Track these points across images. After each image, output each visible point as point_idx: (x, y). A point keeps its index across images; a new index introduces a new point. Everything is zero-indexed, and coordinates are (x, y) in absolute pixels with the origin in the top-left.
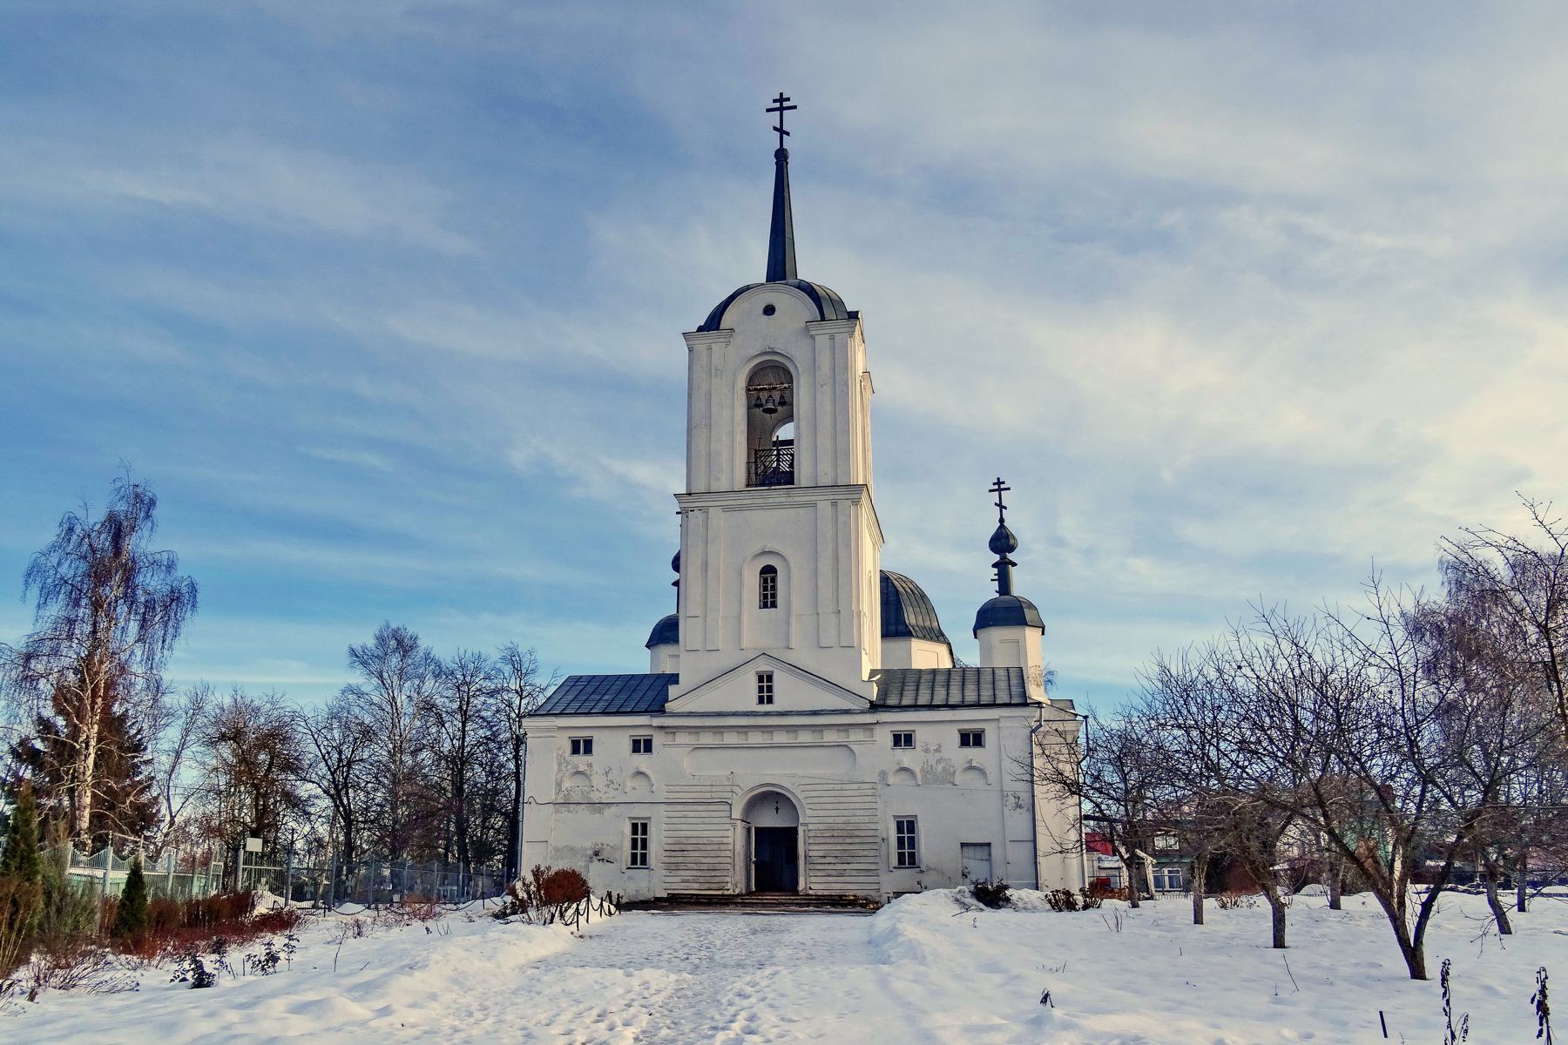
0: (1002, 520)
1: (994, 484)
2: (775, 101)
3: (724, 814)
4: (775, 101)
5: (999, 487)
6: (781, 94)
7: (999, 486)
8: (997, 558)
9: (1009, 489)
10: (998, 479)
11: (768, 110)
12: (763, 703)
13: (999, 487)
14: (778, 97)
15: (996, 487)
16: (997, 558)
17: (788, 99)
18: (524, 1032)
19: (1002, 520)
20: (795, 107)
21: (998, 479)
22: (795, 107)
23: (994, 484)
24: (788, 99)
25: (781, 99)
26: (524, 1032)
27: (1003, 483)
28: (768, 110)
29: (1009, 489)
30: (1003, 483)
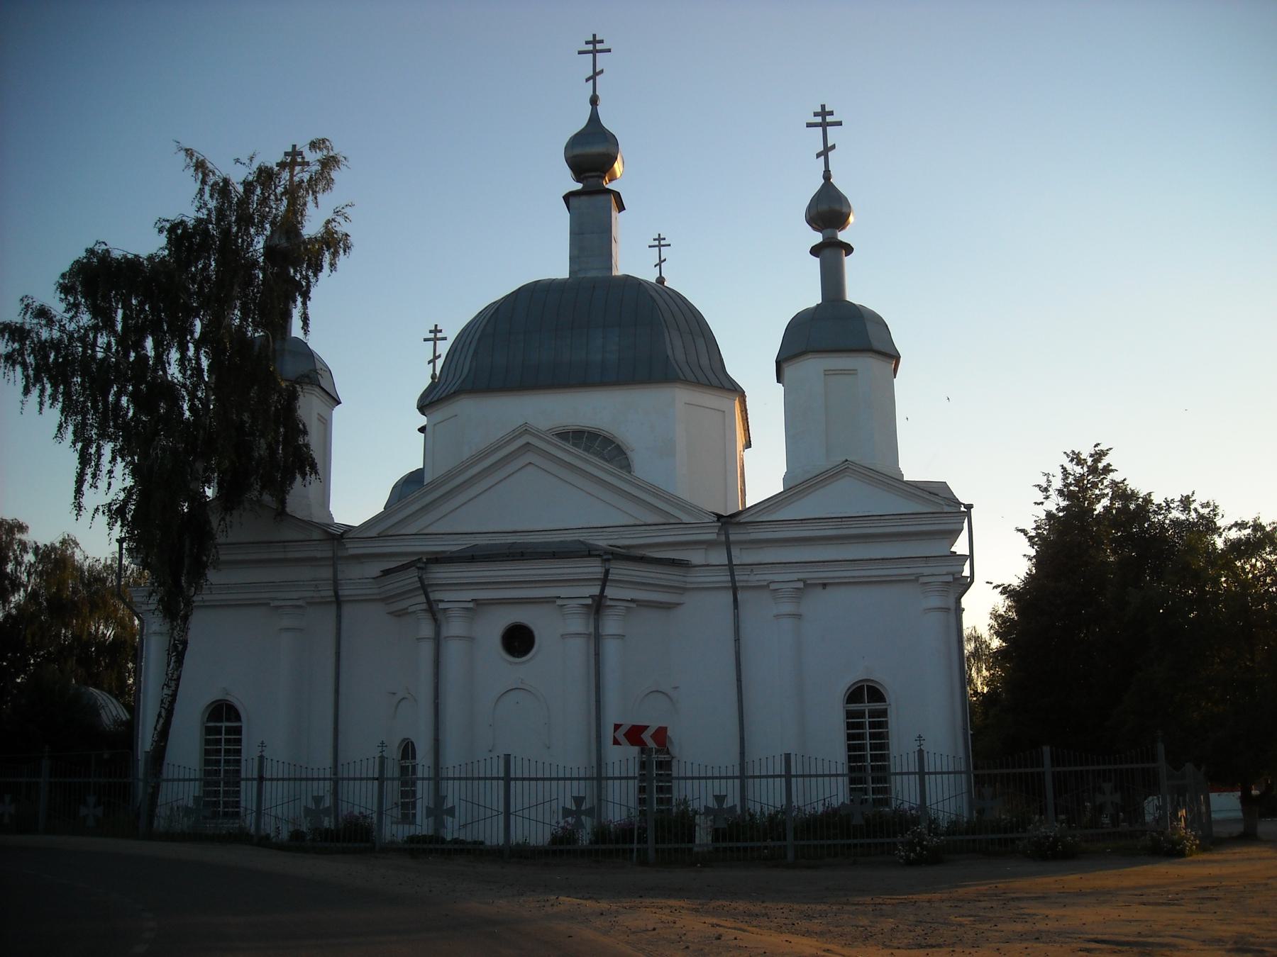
0: (827, 175)
1: (816, 114)
2: (587, 43)
3: (364, 771)
4: (587, 43)
5: (824, 119)
6: (594, 36)
7: (824, 119)
8: (817, 238)
9: (840, 124)
10: (823, 107)
11: (580, 53)
12: (848, 729)
13: (824, 119)
14: (591, 39)
15: (819, 119)
16: (817, 238)
17: (602, 42)
18: (1000, 589)
19: (827, 175)
20: (609, 51)
21: (823, 107)
22: (609, 51)
23: (816, 114)
24: (602, 42)
25: (595, 41)
26: (1000, 589)
27: (831, 113)
28: (580, 53)
29: (840, 124)
30: (831, 113)
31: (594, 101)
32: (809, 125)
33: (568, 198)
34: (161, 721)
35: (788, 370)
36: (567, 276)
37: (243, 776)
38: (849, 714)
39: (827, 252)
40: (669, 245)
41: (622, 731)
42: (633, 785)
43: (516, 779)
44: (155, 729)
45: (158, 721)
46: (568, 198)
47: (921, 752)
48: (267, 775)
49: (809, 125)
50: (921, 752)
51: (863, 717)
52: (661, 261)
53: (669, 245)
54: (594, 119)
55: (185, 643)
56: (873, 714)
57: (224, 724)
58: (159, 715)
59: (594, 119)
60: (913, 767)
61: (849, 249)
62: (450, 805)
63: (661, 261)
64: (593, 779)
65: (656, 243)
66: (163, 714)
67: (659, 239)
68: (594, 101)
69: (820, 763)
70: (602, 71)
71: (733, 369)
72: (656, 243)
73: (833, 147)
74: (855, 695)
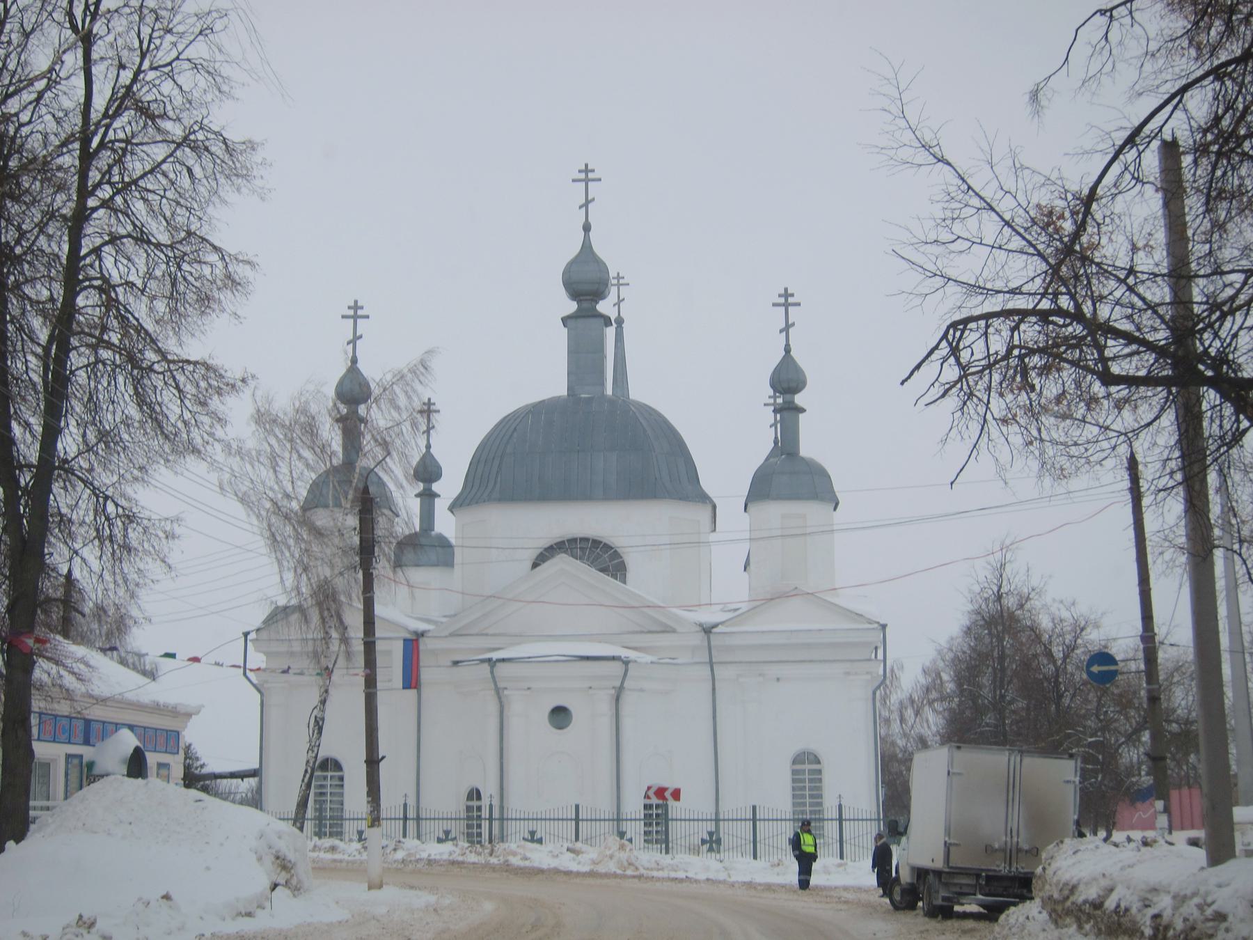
0: (788, 350)
11: (574, 181)
19: (788, 350)
28: (574, 181)
31: (587, 228)
32: (775, 305)
33: (565, 320)
34: (308, 776)
35: (751, 507)
36: (561, 390)
37: (642, 823)
38: (794, 772)
39: (786, 414)
40: (600, 180)
41: (653, 790)
42: (463, 824)
43: (571, 820)
44: (303, 781)
45: (304, 776)
46: (565, 320)
47: (840, 806)
48: (423, 815)
49: (775, 305)
50: (840, 806)
51: (804, 774)
52: (587, 202)
53: (600, 180)
54: (587, 247)
55: (323, 719)
56: (812, 772)
57: (329, 774)
58: (306, 771)
59: (587, 247)
60: (835, 815)
61: (802, 410)
62: (539, 836)
63: (587, 202)
64: (613, 820)
65: (583, 176)
66: (309, 770)
67: (587, 170)
68: (587, 228)
69: (766, 810)
70: (593, 199)
71: (708, 483)
72: (583, 176)
73: (793, 324)
74: (799, 759)
